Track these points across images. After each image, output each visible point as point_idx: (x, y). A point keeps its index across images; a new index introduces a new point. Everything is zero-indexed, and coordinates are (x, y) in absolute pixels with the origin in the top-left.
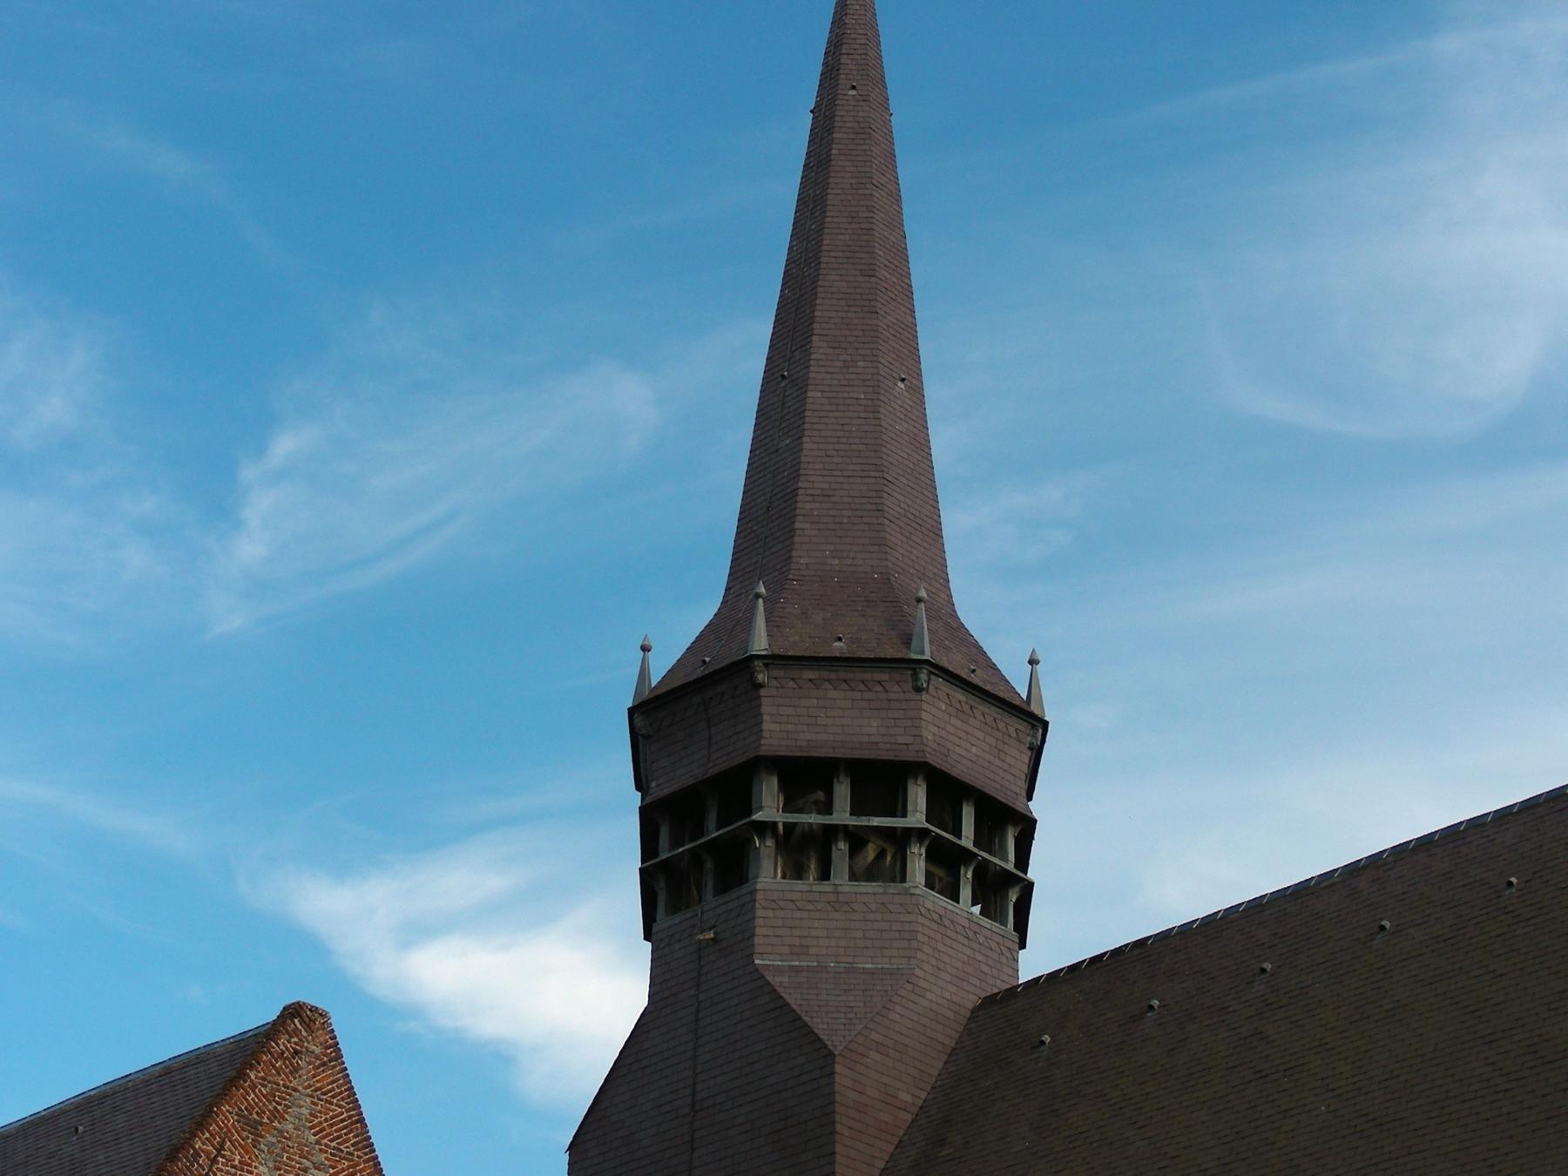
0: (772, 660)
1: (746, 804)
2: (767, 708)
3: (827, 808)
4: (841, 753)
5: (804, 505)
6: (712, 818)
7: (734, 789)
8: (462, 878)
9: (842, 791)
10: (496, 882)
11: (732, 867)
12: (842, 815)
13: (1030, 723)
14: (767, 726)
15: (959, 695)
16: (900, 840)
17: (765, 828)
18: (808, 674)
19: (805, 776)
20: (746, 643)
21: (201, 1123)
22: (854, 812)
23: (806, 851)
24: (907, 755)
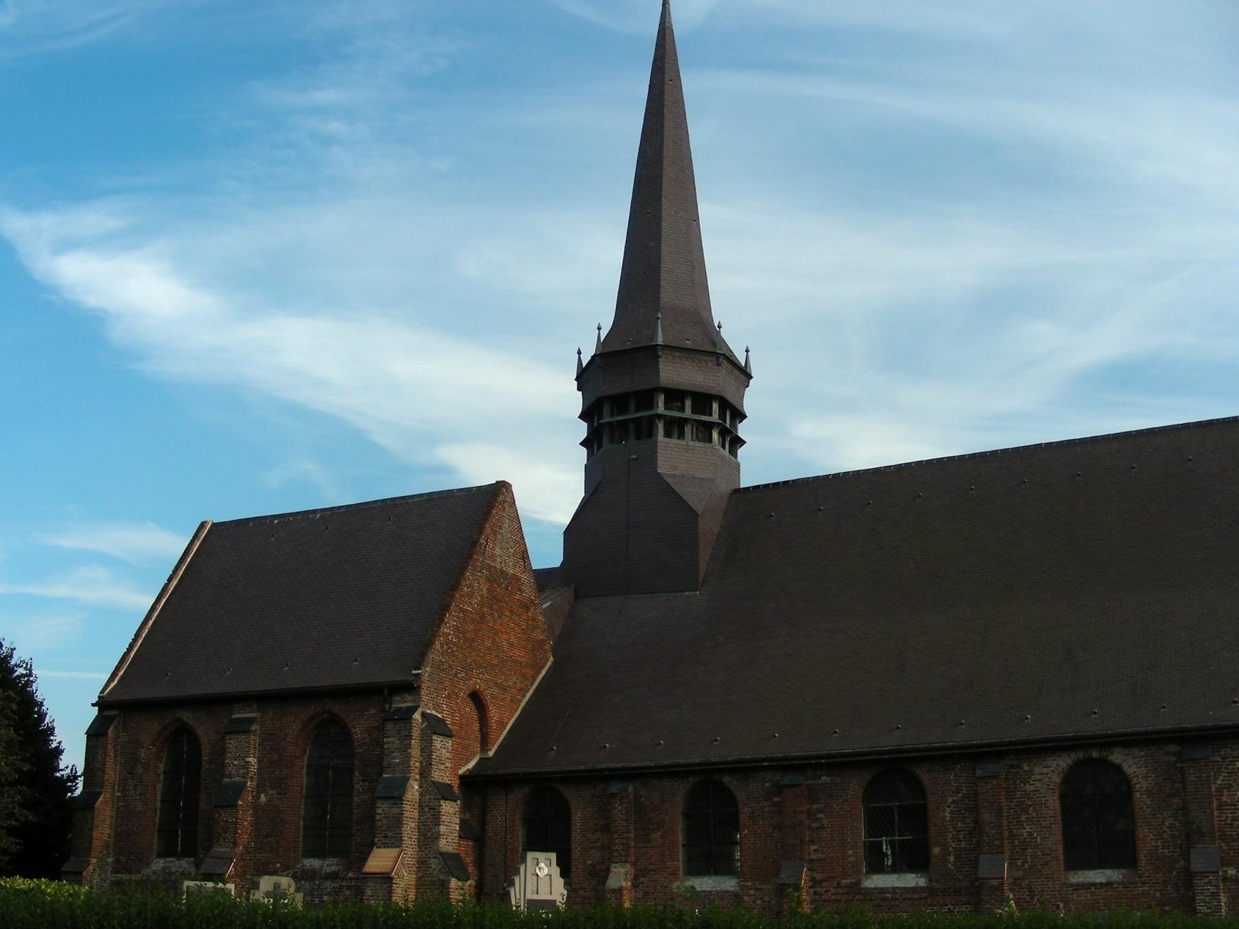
0: (665, 347)
1: (651, 404)
2: (661, 366)
3: (682, 409)
4: (691, 389)
5: (663, 275)
6: (632, 407)
7: (646, 398)
8: (93, 218)
9: (688, 403)
10: (114, 223)
11: (645, 430)
12: (688, 413)
13: (744, 374)
14: (662, 374)
15: (730, 367)
16: (709, 426)
17: (660, 416)
18: (678, 354)
19: (675, 396)
20: (653, 336)
21: (481, 533)
22: (694, 412)
23: (675, 427)
24: (715, 392)
